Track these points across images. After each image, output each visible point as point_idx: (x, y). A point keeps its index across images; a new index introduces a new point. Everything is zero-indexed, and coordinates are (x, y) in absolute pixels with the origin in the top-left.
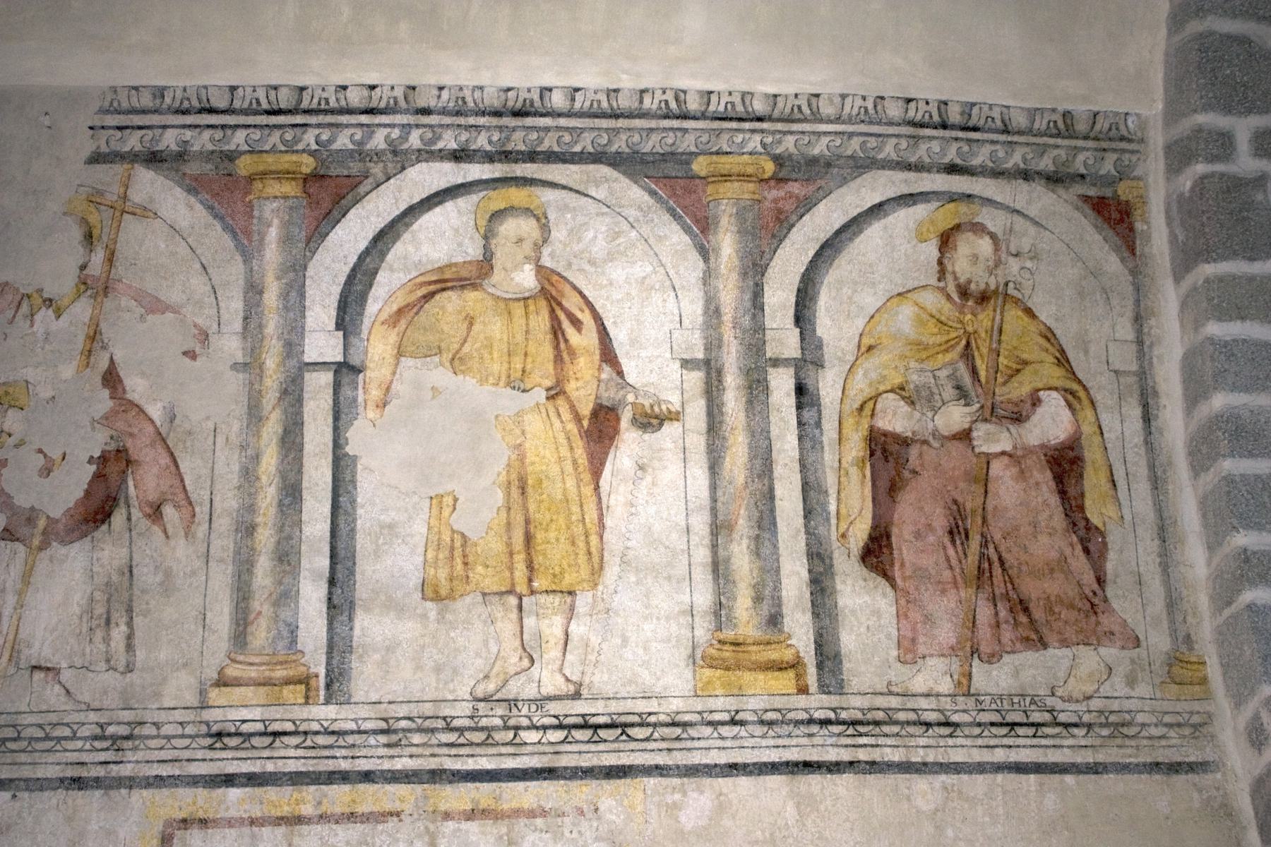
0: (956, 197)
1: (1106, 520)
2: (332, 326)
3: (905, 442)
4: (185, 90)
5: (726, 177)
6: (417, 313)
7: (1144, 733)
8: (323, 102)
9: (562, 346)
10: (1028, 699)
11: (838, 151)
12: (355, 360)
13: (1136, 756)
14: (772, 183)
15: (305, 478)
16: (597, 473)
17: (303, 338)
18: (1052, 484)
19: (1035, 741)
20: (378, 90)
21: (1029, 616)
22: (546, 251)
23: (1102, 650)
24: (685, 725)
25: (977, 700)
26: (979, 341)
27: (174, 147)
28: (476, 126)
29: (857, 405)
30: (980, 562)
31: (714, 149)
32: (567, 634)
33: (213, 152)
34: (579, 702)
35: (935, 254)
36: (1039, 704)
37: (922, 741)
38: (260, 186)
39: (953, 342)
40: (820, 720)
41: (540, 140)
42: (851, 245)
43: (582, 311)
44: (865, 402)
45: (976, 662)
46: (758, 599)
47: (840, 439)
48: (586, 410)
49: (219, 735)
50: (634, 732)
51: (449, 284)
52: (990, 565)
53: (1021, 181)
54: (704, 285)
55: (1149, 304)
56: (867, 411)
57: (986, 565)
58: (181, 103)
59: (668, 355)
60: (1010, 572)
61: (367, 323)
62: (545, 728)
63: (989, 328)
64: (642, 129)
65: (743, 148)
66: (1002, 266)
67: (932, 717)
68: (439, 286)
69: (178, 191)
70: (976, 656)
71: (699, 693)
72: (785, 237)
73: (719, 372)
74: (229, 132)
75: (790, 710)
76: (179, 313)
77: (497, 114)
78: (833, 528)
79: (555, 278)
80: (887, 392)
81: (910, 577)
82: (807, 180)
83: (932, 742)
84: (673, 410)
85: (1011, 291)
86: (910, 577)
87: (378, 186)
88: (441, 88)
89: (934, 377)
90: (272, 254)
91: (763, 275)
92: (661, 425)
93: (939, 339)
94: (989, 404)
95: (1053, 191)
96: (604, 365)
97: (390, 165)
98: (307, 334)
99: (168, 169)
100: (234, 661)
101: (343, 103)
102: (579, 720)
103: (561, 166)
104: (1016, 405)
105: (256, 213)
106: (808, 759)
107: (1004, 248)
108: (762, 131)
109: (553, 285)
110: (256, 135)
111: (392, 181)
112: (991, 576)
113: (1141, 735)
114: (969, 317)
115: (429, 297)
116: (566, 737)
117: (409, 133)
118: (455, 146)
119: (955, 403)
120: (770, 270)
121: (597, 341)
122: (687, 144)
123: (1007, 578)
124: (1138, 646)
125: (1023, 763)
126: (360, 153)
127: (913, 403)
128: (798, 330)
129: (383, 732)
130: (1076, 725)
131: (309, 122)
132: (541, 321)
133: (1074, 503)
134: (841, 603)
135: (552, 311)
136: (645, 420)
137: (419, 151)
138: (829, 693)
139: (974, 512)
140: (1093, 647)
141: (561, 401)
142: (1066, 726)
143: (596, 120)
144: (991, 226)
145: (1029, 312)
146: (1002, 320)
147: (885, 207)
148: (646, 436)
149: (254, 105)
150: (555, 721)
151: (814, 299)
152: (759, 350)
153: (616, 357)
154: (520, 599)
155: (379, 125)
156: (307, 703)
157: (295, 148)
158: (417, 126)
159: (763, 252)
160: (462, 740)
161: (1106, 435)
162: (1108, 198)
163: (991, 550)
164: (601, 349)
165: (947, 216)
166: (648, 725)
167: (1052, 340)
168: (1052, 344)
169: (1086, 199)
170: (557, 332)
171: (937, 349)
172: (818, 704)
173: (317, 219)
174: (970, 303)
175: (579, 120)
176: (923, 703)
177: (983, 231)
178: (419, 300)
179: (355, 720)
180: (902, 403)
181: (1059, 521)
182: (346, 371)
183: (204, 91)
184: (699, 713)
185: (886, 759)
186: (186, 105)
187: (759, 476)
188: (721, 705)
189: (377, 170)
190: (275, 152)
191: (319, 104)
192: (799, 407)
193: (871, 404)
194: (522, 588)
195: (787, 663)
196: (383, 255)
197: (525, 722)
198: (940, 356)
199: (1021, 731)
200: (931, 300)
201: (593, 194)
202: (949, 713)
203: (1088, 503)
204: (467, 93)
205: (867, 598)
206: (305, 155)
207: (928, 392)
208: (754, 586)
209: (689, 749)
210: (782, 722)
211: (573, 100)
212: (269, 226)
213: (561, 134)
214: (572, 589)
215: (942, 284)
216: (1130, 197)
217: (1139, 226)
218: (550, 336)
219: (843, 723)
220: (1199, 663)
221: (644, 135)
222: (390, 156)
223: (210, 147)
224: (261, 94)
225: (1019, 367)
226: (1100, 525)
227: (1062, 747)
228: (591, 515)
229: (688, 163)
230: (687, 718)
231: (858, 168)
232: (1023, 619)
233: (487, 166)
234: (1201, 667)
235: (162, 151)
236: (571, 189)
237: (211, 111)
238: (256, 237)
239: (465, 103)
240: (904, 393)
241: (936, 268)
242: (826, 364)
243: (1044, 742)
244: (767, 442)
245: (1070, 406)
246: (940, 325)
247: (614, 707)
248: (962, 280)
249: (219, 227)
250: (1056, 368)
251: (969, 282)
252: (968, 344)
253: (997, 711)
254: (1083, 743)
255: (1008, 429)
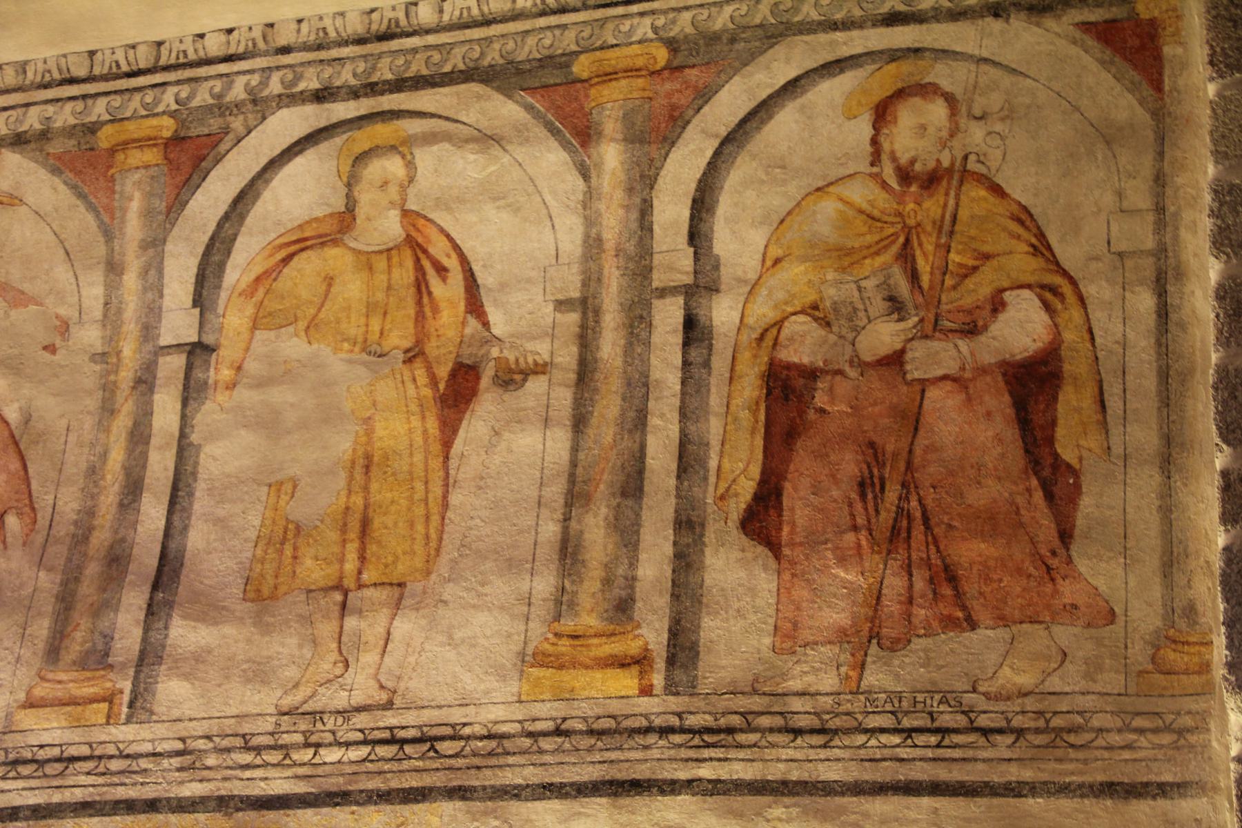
0: (899, 54)
1: (1085, 454)
2: (189, 302)
3: (812, 374)
4: (45, 62)
5: (609, 76)
6: (275, 280)
7: (1100, 742)
8: (181, 56)
9: (425, 300)
10: (937, 697)
11: (744, 22)
12: (209, 339)
13: (1081, 773)
14: (666, 74)
15: (148, 474)
16: (447, 444)
17: (160, 321)
18: (1010, 411)
19: (941, 752)
20: (235, 33)
21: (956, 588)
22: (412, 191)
23: (1057, 630)
24: (503, 736)
25: (867, 699)
26: (922, 236)
27: (37, 126)
28: (339, 59)
29: (755, 335)
30: (896, 520)
31: (598, 43)
32: (389, 633)
33: (75, 126)
34: (389, 713)
35: (868, 131)
36: (952, 703)
37: (790, 753)
38: (122, 156)
39: (885, 242)
40: (661, 728)
41: (408, 63)
42: (758, 136)
43: (448, 256)
44: (766, 330)
45: (874, 649)
46: (607, 582)
47: (731, 378)
48: (443, 372)
49: (16, 762)
50: (443, 747)
51: (309, 243)
52: (909, 523)
53: (989, 20)
54: (585, 209)
55: (1179, 154)
56: (769, 341)
57: (905, 523)
58: (43, 77)
59: (540, 298)
60: (936, 531)
61: (224, 295)
62: (348, 744)
63: (938, 217)
64: (517, 33)
65: (631, 37)
66: (960, 135)
67: (803, 722)
68: (297, 247)
69: (43, 174)
70: (874, 641)
71: (524, 698)
72: (679, 137)
73: (597, 312)
74: (90, 102)
75: (627, 717)
76: (41, 305)
77: (360, 41)
78: (711, 489)
79: (422, 221)
80: (795, 314)
81: (801, 544)
82: (708, 63)
83: (799, 755)
84: (541, 362)
85: (972, 165)
86: (801, 544)
87: (239, 141)
88: (300, 21)
89: (859, 289)
90: (133, 228)
91: (652, 188)
92: (525, 380)
93: (869, 239)
94: (931, 317)
95: (1038, 25)
96: (469, 316)
97: (250, 116)
98: (164, 315)
99: (33, 150)
100: (43, 679)
101: (202, 54)
102: (386, 735)
103: (430, 91)
104: (970, 312)
105: (117, 188)
106: (637, 776)
107: (964, 110)
108: (653, 12)
109: (418, 230)
110: (117, 101)
111: (253, 134)
112: (909, 537)
113: (1095, 744)
114: (912, 206)
115: (286, 260)
116: (369, 754)
117: (269, 78)
118: (317, 86)
119: (885, 318)
120: (660, 181)
121: (462, 290)
122: (568, 41)
123: (930, 538)
124: (1112, 622)
125: (917, 782)
126: (221, 108)
127: (828, 324)
128: (692, 249)
129: (179, 753)
130: (1000, 731)
131: (168, 80)
132: (404, 274)
133: (1039, 434)
134: (708, 581)
135: (417, 261)
136: (507, 378)
137: (280, 96)
138: (677, 694)
139: (895, 455)
140: (1044, 626)
141: (418, 364)
142: (985, 732)
143: (467, 31)
144: (946, 85)
145: (997, 190)
146: (957, 205)
147: (803, 82)
148: (506, 396)
149: (114, 70)
150: (359, 736)
151: (711, 210)
152: (645, 278)
153: (482, 306)
154: (346, 595)
155: (239, 73)
156: (108, 723)
157: (156, 111)
158: (278, 68)
159: (652, 161)
160: (258, 761)
161: (1098, 341)
162: (1121, 21)
163: (914, 503)
164: (467, 299)
165: (885, 79)
166: (461, 738)
167: (1028, 223)
168: (1027, 228)
169: (1086, 27)
170: (421, 285)
171: (865, 252)
172: (657, 707)
173: (177, 187)
174: (914, 188)
175: (448, 34)
176: (797, 704)
177: (935, 93)
178: (277, 265)
179: (152, 741)
180: (815, 325)
181: (1016, 457)
182: (199, 351)
183: (63, 60)
184: (519, 722)
185: (735, 777)
186: (47, 78)
187: (630, 431)
188: (547, 711)
189: (237, 124)
190: (137, 118)
191: (178, 58)
192: (686, 344)
193: (774, 331)
194: (349, 582)
195: (632, 657)
196: (242, 218)
197: (329, 738)
198: (867, 261)
199: (920, 739)
200: (861, 193)
201: (464, 119)
202: (827, 717)
203: (1060, 432)
204: (327, 22)
205: (743, 574)
206: (165, 117)
207: (850, 309)
208: (606, 565)
209: (500, 767)
210: (615, 732)
211: (441, 11)
212: (131, 200)
213: (429, 54)
214: (403, 580)
215: (875, 170)
216: (1156, 13)
217: (1168, 50)
218: (413, 290)
219: (690, 731)
220: (1202, 644)
221: (519, 40)
222: (250, 106)
223: (72, 121)
224: (120, 56)
225: (976, 263)
226: (1074, 462)
227: (976, 760)
228: (437, 490)
229: (568, 65)
230: (504, 728)
231: (768, 38)
232: (947, 591)
233: (352, 104)
234: (1203, 649)
235: (26, 132)
236: (440, 117)
237: (72, 81)
238: (118, 214)
239: (326, 34)
240: (817, 313)
241: (869, 149)
242: (723, 287)
243: (948, 753)
244: (644, 390)
245: (1047, 306)
246: (870, 221)
247: (428, 716)
248: (904, 159)
249: (82, 209)
250: (1030, 259)
251: (913, 162)
252: (907, 241)
253: (892, 712)
254: (1008, 754)
255: (956, 346)
